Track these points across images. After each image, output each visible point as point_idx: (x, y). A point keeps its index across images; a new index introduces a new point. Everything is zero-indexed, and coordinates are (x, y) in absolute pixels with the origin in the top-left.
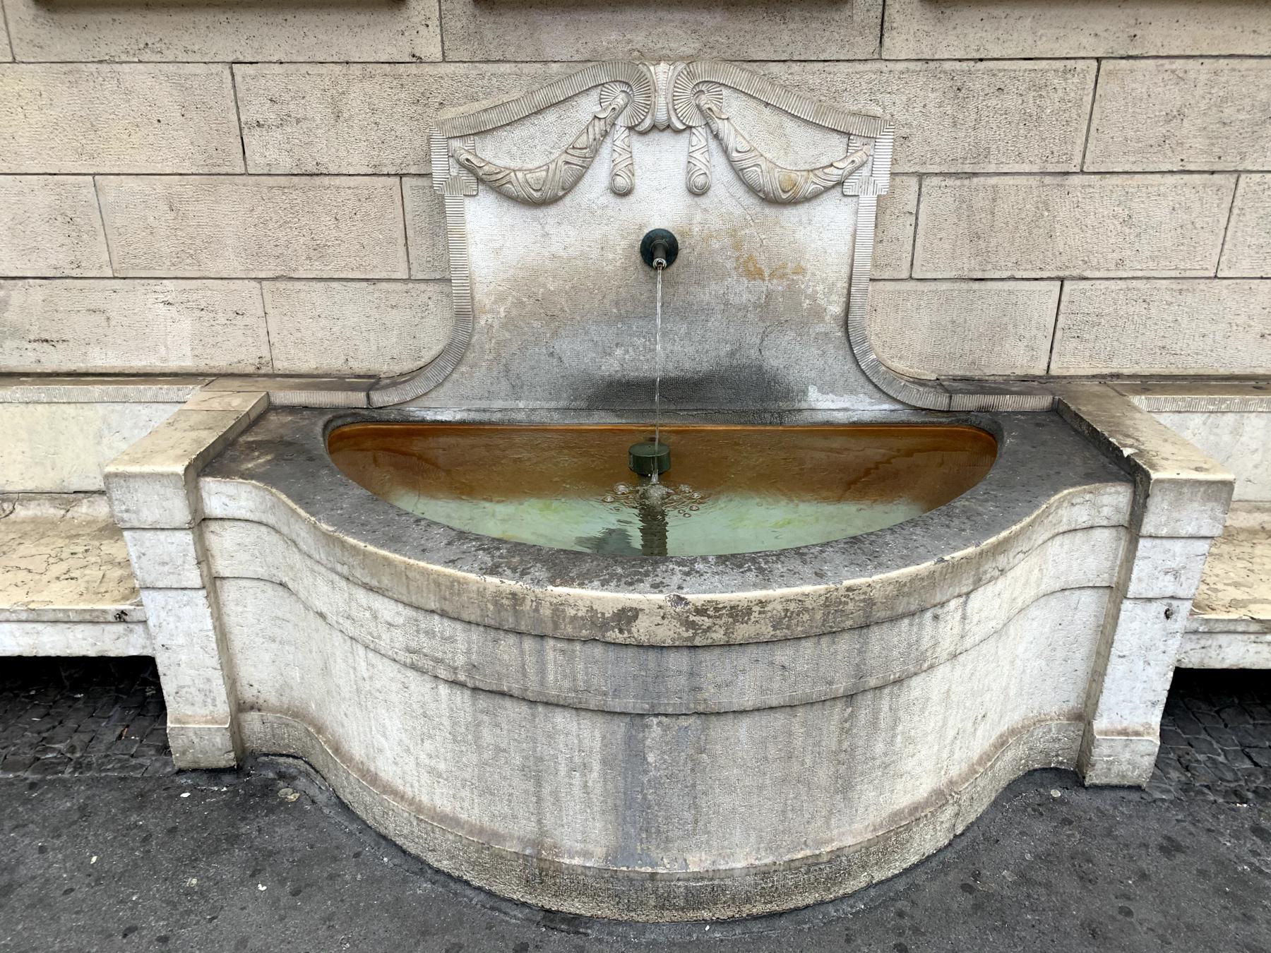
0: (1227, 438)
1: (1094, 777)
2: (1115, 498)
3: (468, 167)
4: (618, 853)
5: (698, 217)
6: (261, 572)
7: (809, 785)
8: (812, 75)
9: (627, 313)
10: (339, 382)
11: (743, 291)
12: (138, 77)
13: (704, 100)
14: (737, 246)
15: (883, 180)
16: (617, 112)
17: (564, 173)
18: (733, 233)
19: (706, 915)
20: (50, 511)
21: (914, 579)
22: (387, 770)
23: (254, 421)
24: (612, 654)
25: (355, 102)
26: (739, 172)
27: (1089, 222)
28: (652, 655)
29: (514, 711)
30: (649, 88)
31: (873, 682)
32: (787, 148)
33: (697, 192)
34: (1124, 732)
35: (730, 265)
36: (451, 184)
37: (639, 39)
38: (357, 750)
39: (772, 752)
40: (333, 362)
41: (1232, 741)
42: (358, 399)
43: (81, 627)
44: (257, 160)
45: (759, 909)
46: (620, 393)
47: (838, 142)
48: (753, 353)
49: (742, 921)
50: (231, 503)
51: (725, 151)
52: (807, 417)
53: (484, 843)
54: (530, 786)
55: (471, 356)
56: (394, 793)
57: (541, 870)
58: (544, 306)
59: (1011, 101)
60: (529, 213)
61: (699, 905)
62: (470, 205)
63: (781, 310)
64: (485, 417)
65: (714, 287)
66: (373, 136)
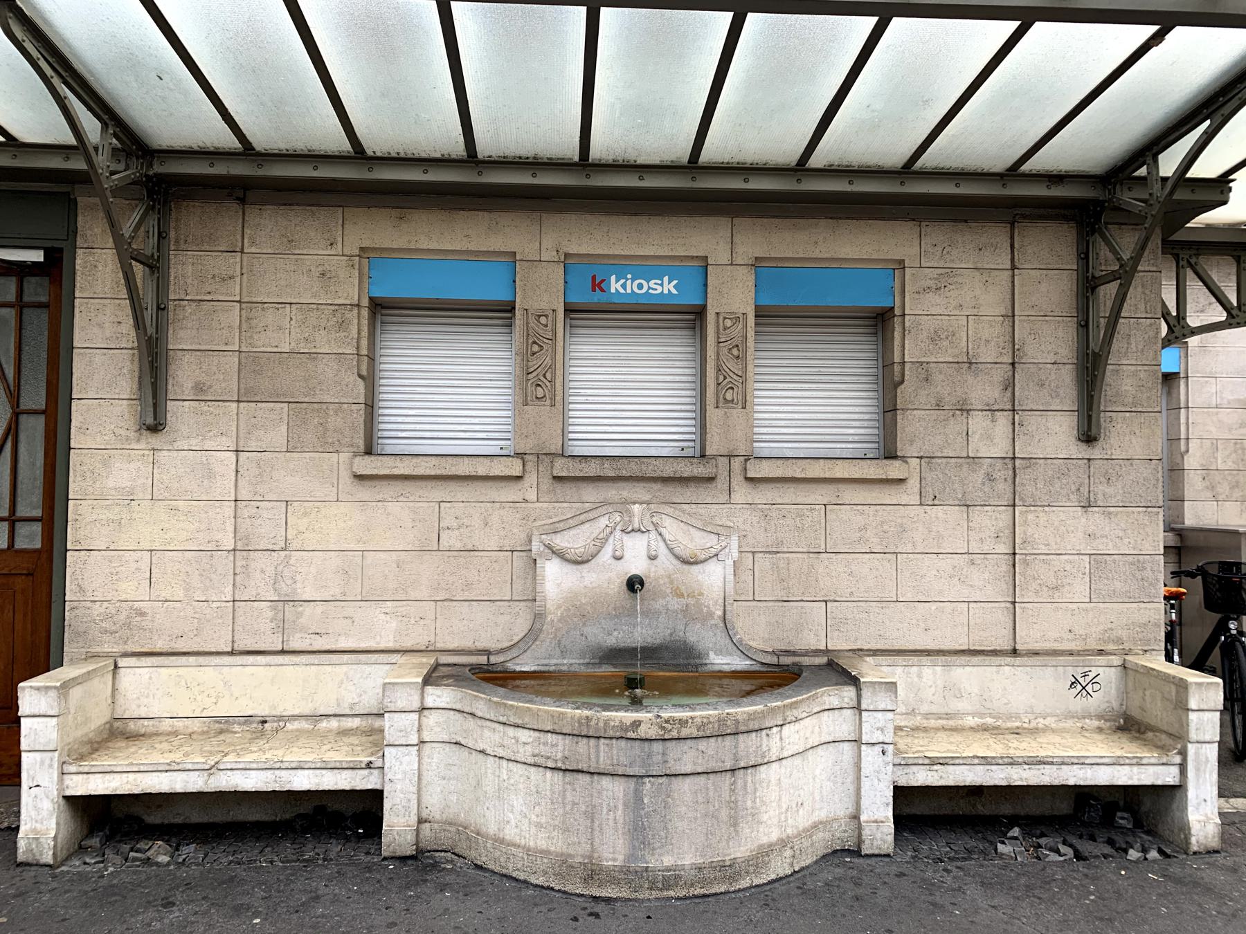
0: (916, 679)
1: (866, 850)
2: (849, 692)
3: (549, 547)
4: (631, 857)
5: (653, 569)
6: (446, 738)
7: (717, 819)
8: (702, 509)
9: (623, 614)
10: (470, 652)
11: (675, 603)
12: (393, 507)
13: (654, 519)
14: (671, 582)
15: (735, 554)
16: (616, 524)
17: (593, 549)
18: (669, 577)
19: (672, 893)
20: (304, 725)
21: (755, 712)
22: (510, 833)
23: (436, 666)
24: (630, 743)
25: (495, 519)
26: (671, 550)
27: (833, 574)
28: (646, 744)
29: (583, 779)
30: (631, 515)
31: (742, 765)
32: (692, 540)
33: (652, 558)
34: (876, 821)
35: (668, 591)
36: (540, 554)
37: (625, 494)
38: (492, 829)
39: (700, 800)
40: (467, 644)
41: (943, 842)
42: (483, 659)
43: (346, 772)
44: (445, 544)
45: (698, 891)
46: (614, 655)
47: (714, 537)
48: (681, 634)
49: (690, 898)
50: (438, 700)
51: (665, 541)
52: (709, 668)
53: (564, 865)
54: (588, 822)
55: (542, 636)
56: (514, 845)
57: (592, 873)
58: (579, 612)
59: (789, 521)
60: (575, 567)
61: (667, 887)
62: (548, 564)
63: (693, 613)
64: (546, 668)
65: (661, 602)
66: (502, 533)
